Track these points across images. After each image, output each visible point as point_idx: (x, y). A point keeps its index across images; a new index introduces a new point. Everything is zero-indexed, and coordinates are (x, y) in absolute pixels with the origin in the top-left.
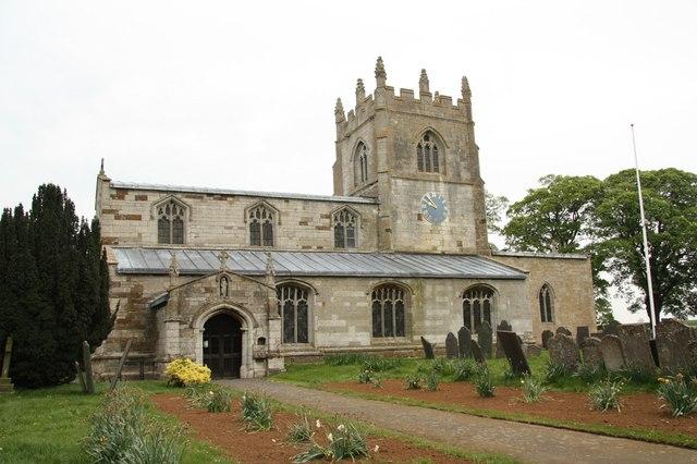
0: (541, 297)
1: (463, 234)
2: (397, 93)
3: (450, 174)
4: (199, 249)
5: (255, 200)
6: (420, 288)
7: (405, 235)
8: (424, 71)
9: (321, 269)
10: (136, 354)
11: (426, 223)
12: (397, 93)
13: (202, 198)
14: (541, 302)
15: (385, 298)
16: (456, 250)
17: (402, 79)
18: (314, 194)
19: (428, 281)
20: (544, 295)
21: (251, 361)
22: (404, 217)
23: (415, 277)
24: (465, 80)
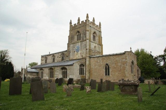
0: (106, 67)
3: (81, 39)
4: (90, 61)
6: (55, 68)
7: (72, 56)
8: (79, 18)
9: (66, 64)
11: (76, 53)
14: (51, 73)
16: (81, 57)
17: (75, 22)
19: (56, 67)
20: (107, 67)
22: (72, 52)
23: (54, 66)
24: (87, 15)
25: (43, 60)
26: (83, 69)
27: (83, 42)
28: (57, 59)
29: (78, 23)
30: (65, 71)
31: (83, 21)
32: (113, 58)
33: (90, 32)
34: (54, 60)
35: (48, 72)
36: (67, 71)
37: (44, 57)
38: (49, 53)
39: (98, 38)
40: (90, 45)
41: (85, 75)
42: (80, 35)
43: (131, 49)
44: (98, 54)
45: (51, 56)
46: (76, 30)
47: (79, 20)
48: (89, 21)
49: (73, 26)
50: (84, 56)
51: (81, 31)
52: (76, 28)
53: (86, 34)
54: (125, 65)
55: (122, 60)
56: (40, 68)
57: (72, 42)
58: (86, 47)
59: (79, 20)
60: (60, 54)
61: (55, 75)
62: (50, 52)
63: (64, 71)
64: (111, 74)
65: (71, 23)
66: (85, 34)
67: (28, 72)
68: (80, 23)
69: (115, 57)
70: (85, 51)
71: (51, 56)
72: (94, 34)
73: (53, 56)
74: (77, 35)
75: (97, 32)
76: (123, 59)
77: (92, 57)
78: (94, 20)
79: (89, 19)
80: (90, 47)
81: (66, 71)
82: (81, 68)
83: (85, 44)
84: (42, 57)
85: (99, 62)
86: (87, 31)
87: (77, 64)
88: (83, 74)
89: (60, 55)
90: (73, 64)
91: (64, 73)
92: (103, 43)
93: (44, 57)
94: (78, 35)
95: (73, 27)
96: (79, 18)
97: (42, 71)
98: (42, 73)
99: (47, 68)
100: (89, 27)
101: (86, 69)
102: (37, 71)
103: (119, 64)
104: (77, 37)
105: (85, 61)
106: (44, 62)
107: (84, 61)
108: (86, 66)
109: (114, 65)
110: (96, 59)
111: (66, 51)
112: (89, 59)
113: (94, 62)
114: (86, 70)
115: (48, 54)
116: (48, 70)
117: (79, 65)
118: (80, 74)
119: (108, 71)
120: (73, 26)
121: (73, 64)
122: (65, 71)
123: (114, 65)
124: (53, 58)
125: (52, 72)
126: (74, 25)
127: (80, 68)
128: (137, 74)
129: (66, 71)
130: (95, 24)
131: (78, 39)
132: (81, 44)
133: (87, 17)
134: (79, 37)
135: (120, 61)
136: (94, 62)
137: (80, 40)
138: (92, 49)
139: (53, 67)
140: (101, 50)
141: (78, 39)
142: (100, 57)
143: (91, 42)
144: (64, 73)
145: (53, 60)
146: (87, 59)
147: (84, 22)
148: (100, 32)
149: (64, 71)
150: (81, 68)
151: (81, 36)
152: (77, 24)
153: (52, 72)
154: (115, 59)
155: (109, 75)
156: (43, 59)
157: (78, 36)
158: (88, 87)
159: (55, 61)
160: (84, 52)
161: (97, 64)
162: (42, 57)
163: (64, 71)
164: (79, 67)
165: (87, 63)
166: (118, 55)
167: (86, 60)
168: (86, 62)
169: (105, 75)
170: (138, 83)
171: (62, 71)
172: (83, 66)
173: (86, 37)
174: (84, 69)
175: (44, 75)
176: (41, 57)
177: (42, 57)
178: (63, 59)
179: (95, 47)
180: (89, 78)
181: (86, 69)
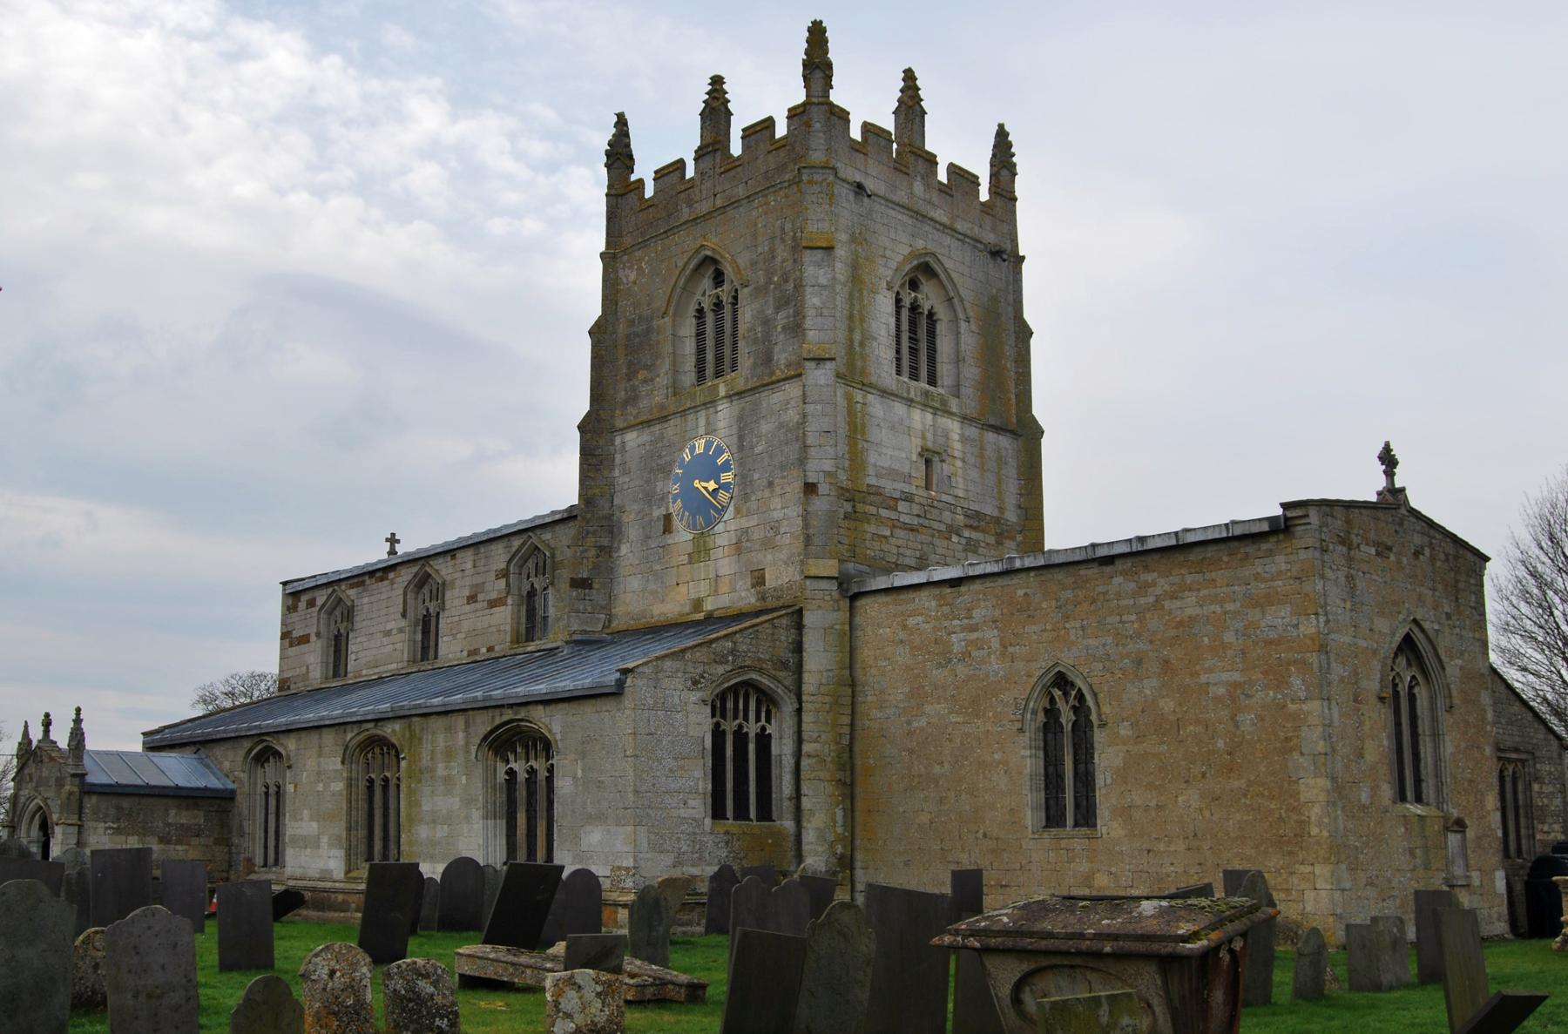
0: (1051, 713)
1: (768, 544)
2: (633, 178)
3: (745, 362)
5: (516, 543)
8: (717, 81)
9: (541, 688)
10: (63, 894)
12: (633, 178)
13: (363, 583)
15: (735, 717)
16: (746, 598)
18: (439, 541)
20: (1067, 717)
21: (1444, 712)
22: (633, 532)
25: (304, 639)
26: (764, 740)
27: (774, 398)
28: (466, 626)
29: (700, 155)
30: (532, 772)
31: (769, 123)
32: (1144, 588)
33: (855, 267)
34: (427, 630)
35: (339, 786)
36: (551, 770)
37: (321, 597)
38: (392, 552)
39: (969, 341)
40: (856, 429)
41: (788, 824)
42: (735, 312)
43: (1390, 474)
44: (971, 547)
45: (392, 593)
46: (684, 247)
47: (716, 108)
48: (842, 116)
49: (649, 192)
50: (781, 574)
51: (738, 258)
52: (686, 213)
53: (799, 286)
54: (1296, 682)
55: (1253, 615)
56: (247, 744)
57: (633, 399)
58: (802, 461)
59: (716, 108)
60: (499, 557)
61: (423, 832)
62: (393, 540)
63: (519, 766)
64: (1124, 813)
65: (619, 155)
66: (791, 298)
67: (88, 790)
68: (736, 148)
69: (1163, 585)
70: (794, 511)
71: (392, 593)
72: (914, 285)
73: (422, 581)
74: (700, 313)
75: (956, 262)
76: (1263, 603)
77: (881, 582)
78: (910, 106)
79: (836, 97)
80: (856, 460)
81: (542, 774)
82: (729, 726)
83: (792, 415)
84: (296, 595)
85: (965, 656)
86: (808, 257)
87: (678, 682)
88: (765, 813)
89: (504, 574)
90: (620, 684)
91: (521, 793)
92: (1042, 408)
93: (311, 603)
94: (707, 305)
95: (651, 204)
96: (717, 81)
97: (270, 772)
98: (275, 799)
99: (329, 738)
100: (845, 192)
101: (799, 741)
102: (214, 783)
103: (1219, 677)
104: (700, 335)
105: (785, 637)
106: (314, 658)
107: (765, 646)
108: (799, 711)
109: (1149, 686)
110: (925, 610)
111: (569, 516)
112: (839, 617)
113: (902, 656)
114: (805, 763)
115: (377, 554)
116: (334, 763)
117: (707, 694)
118: (718, 813)
119: (746, 760)
120: (649, 192)
121: (620, 684)
122: (532, 772)
123: (1155, 682)
124: (416, 611)
125: (385, 787)
126: (660, 175)
127: (718, 735)
128: (1491, 801)
129: (539, 765)
130: (931, 160)
131: (710, 356)
132: (744, 429)
133: (817, 66)
134: (719, 331)
135: (1229, 637)
136: (902, 656)
137: (734, 367)
138: (890, 487)
139: (392, 731)
140: (1011, 500)
141: (710, 356)
142: (977, 586)
143: (867, 386)
144: (521, 793)
145: (426, 632)
146: (809, 619)
147: (781, 130)
148: (996, 254)
149: (522, 776)
150: (729, 726)
151: (747, 314)
152: (690, 172)
153: (385, 787)
154: (1157, 605)
155: (1086, 816)
156: (309, 622)
157: (710, 318)
158: (572, 983)
159: (443, 650)
160: (775, 528)
161: (939, 675)
162: (296, 595)
163: (522, 776)
164: (700, 724)
165: (818, 661)
166: (1194, 556)
167: (799, 626)
168: (798, 648)
169: (1031, 817)
170: (1213, 927)
171: (502, 776)
172: (767, 701)
173: (796, 328)
174: (782, 749)
175: (298, 825)
176: (278, 594)
177: (296, 595)
178: (532, 623)
179: (929, 458)
180: (846, 863)
181: (799, 741)
